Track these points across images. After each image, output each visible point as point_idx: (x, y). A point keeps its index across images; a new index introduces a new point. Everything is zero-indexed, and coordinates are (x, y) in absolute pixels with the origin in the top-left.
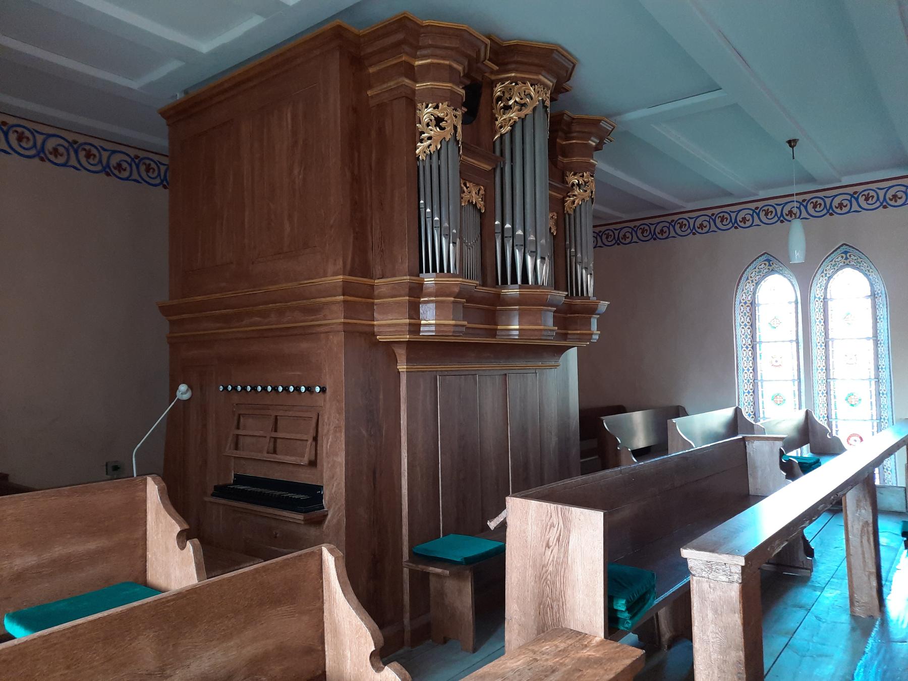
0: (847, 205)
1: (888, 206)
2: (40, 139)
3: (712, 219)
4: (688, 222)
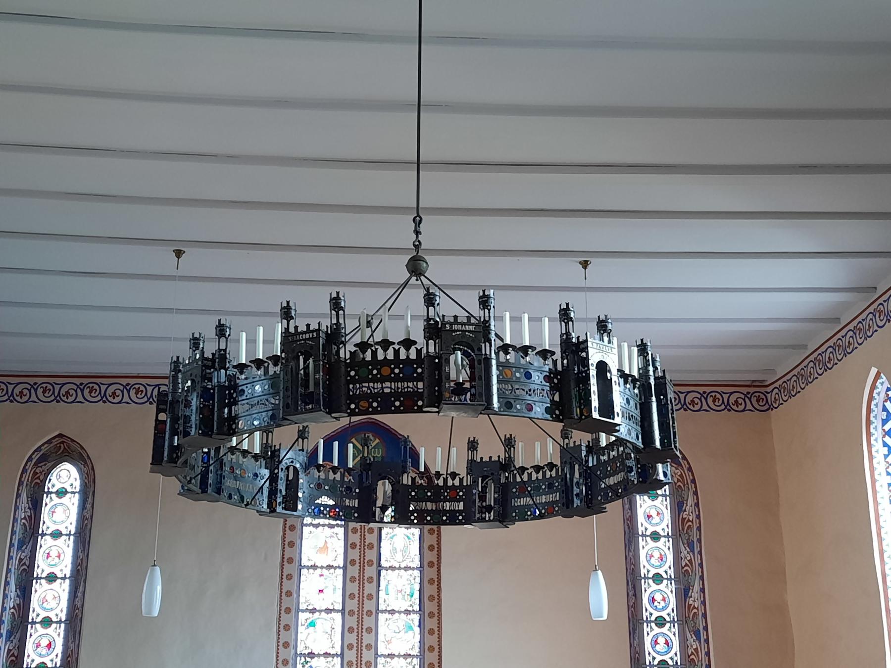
0: (26, 394)
1: (107, 402)
2: (726, 397)
3: (34, 388)
4: (100, 387)
